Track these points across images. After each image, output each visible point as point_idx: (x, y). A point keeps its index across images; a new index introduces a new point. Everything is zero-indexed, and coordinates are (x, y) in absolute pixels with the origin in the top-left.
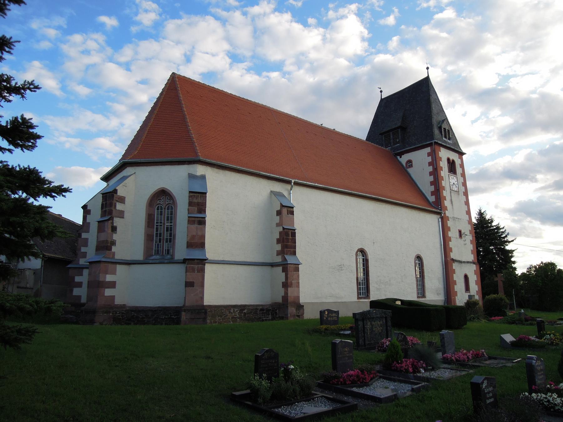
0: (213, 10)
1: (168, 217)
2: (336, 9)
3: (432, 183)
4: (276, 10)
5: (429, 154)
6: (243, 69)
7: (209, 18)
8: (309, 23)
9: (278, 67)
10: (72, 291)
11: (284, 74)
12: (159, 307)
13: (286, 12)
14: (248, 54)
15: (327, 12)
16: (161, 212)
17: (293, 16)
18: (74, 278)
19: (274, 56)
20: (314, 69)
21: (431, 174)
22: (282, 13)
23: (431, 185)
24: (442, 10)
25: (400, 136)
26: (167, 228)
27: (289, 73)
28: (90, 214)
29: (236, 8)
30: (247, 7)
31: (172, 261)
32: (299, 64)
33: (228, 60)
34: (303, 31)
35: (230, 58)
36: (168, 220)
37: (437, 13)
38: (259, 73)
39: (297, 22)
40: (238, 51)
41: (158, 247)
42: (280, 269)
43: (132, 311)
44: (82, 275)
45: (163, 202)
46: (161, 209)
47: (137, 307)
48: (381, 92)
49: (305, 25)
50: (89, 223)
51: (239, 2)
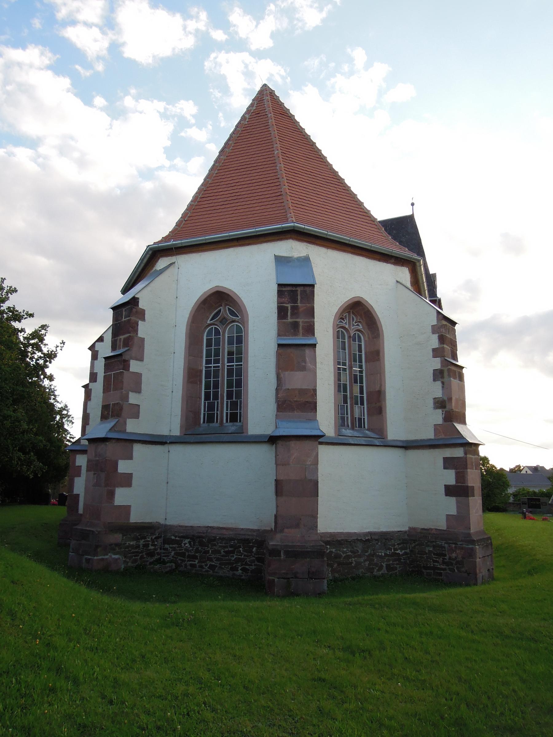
2: (137, 98)
3: (436, 353)
4: (49, 67)
9: (32, 143)
10: (112, 494)
12: (370, 533)
17: (74, 84)
19: (29, 126)
20: (82, 163)
23: (435, 356)
28: (434, 350)
30: (7, 47)
31: (241, 438)
32: (63, 150)
44: (130, 457)
45: (354, 326)
50: (143, 340)
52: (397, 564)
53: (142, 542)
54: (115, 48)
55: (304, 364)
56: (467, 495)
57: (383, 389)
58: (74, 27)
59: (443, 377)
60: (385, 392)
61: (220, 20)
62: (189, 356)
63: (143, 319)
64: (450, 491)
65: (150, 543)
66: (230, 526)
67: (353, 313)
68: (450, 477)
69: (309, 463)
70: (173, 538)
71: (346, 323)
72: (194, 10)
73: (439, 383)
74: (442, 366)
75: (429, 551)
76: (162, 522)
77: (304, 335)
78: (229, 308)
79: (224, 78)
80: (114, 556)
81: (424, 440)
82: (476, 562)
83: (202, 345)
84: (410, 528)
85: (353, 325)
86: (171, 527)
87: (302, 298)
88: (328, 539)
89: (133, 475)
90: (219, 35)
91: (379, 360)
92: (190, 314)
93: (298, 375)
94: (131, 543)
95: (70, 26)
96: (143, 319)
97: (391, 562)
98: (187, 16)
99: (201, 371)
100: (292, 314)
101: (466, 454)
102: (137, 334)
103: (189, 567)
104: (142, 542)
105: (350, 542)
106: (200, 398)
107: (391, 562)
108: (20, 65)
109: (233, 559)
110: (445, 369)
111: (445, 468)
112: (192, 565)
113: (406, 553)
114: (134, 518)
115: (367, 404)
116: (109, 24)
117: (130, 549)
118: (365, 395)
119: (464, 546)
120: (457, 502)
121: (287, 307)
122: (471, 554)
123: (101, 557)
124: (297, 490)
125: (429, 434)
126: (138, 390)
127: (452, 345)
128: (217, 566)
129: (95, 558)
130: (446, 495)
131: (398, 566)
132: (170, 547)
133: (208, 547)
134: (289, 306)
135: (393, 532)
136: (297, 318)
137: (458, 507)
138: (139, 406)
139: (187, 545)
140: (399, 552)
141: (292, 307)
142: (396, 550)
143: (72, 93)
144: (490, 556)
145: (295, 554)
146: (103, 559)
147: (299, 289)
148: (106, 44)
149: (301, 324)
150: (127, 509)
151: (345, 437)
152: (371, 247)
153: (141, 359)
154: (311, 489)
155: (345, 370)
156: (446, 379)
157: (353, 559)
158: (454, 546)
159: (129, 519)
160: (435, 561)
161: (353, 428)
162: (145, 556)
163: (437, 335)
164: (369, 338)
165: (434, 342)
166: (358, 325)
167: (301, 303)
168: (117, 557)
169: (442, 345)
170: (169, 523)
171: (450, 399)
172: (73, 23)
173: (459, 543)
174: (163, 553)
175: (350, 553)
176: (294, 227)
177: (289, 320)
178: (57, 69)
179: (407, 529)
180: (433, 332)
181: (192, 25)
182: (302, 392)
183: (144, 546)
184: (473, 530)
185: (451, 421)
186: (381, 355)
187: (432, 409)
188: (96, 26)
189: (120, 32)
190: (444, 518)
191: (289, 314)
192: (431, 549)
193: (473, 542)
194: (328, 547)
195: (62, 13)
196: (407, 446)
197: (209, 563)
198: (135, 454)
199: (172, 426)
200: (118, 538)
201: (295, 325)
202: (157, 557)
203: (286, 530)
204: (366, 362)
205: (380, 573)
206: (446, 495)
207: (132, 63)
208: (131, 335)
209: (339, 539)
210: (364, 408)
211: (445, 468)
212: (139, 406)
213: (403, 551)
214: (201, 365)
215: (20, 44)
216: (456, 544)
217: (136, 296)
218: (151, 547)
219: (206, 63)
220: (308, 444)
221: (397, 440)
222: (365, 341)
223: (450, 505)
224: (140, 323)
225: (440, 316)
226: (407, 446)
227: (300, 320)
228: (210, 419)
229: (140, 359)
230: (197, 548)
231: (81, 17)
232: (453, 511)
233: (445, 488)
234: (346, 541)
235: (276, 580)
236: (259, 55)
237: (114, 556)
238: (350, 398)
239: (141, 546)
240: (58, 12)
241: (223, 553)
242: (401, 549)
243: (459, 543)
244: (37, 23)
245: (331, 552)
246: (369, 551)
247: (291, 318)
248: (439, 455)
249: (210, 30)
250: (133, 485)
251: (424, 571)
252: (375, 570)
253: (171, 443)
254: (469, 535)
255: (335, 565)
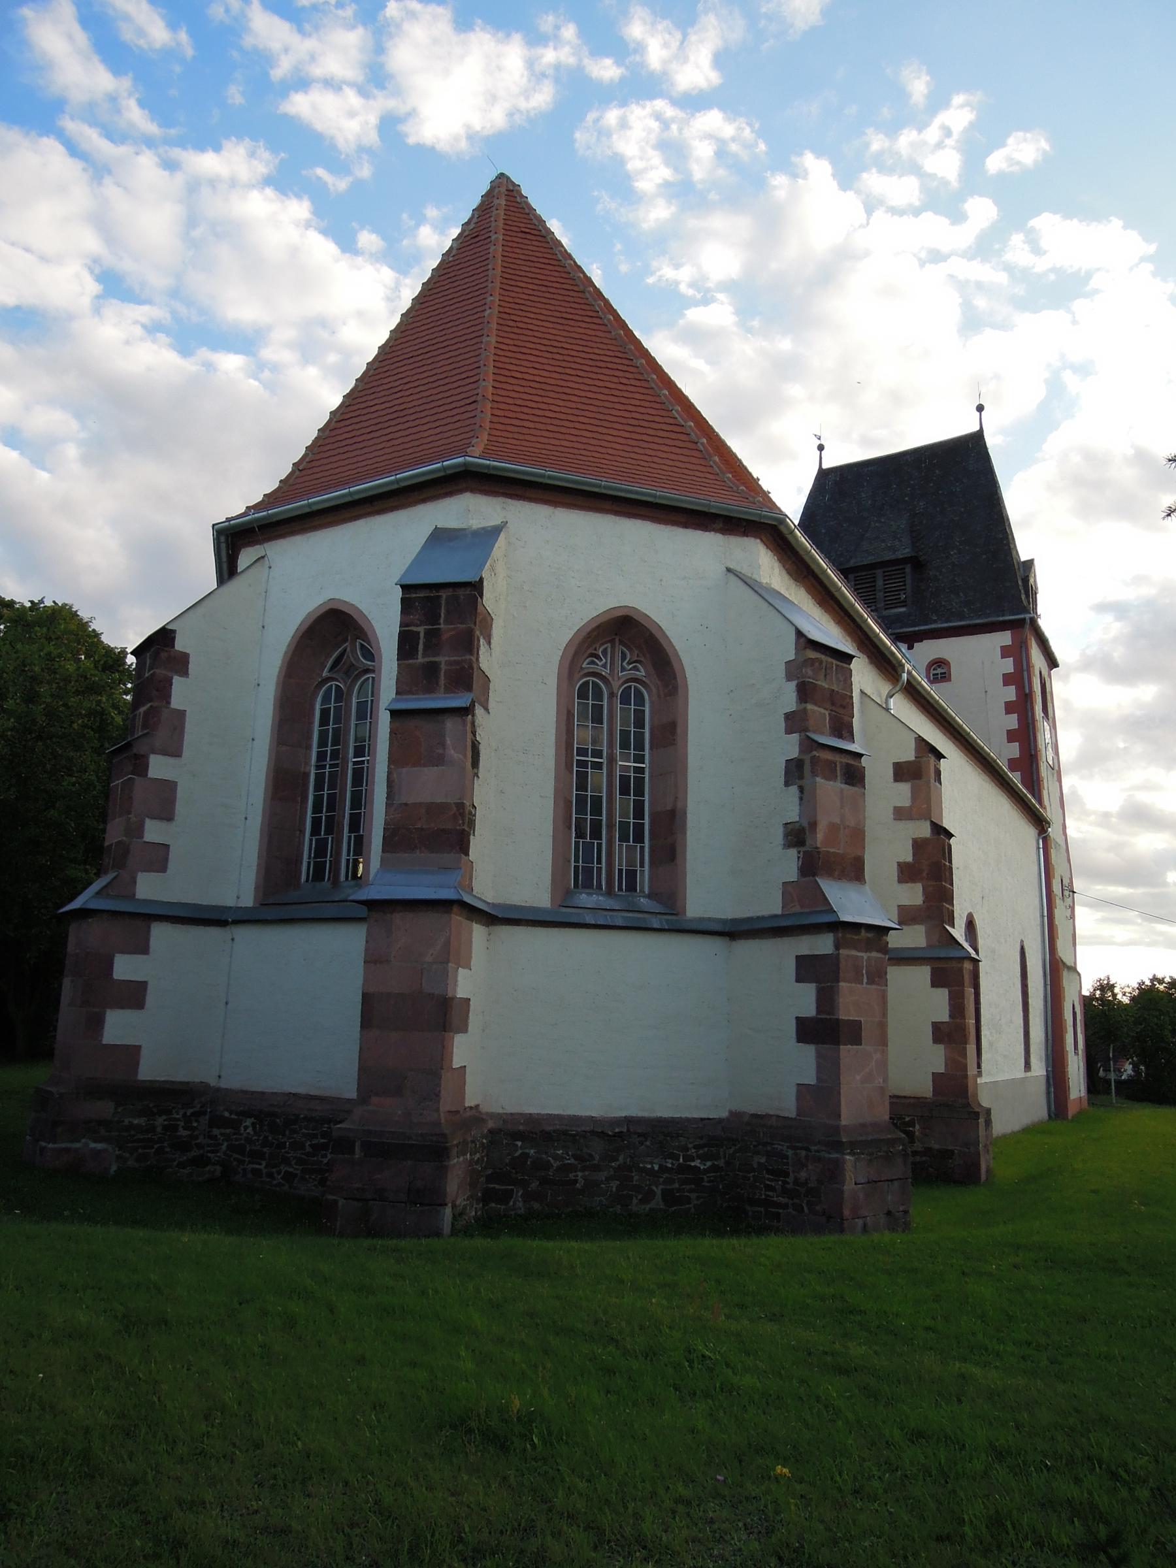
0: (71, 126)
1: (625, 735)
4: (268, 181)
5: (1005, 652)
6: (136, 322)
7: (51, 145)
8: (360, 245)
9: (244, 341)
10: (96, 1023)
11: (258, 368)
12: (629, 1120)
13: (298, 196)
14: (159, 281)
15: (418, 226)
16: (598, 709)
17: (317, 212)
18: (108, 965)
19: (241, 308)
21: (1009, 708)
22: (286, 195)
23: (1009, 741)
24: (706, 300)
25: (908, 587)
26: (624, 780)
27: (275, 368)
28: (788, 717)
29: (149, 142)
30: (185, 148)
33: (93, 287)
34: (337, 260)
35: (99, 279)
36: (625, 745)
37: (696, 303)
38: (185, 351)
39: (325, 232)
40: (126, 265)
41: (588, 859)
42: (923, 973)
43: (516, 1135)
44: (144, 949)
45: (619, 669)
46: (598, 695)
47: (531, 1119)
48: (821, 448)
49: (347, 245)
50: (182, 714)
51: (160, 126)
52: (691, 1191)
53: (160, 1121)
54: (391, 126)
55: (440, 751)
56: (836, 1041)
57: (679, 805)
58: (306, 93)
59: (801, 777)
60: (685, 813)
61: (604, 37)
62: (279, 744)
63: (184, 673)
64: (807, 1031)
65: (182, 1124)
66: (327, 1094)
67: (621, 642)
68: (805, 1000)
69: (429, 959)
70: (227, 1114)
71: (604, 666)
72: (547, 22)
73: (794, 790)
74: (801, 752)
75: (759, 1163)
76: (213, 1082)
77: (448, 690)
78: (362, 646)
79: (619, 161)
80: (93, 1145)
81: (762, 918)
82: (842, 1192)
83: (311, 723)
84: (731, 1113)
85: (623, 669)
86: (228, 1091)
87: (448, 612)
88: (521, 1128)
89: (149, 987)
90: (607, 70)
91: (673, 743)
92: (283, 660)
93: (429, 774)
94: (136, 1122)
95: (297, 92)
96: (184, 673)
97: (677, 1185)
98: (535, 39)
99: (307, 775)
100: (427, 647)
101: (837, 946)
102: (169, 703)
103: (250, 1176)
104: (160, 1121)
105: (574, 1135)
106: (302, 832)
107: (677, 1185)
108: (213, 182)
109: (325, 1161)
110: (807, 758)
111: (798, 981)
112: (254, 1171)
113: (714, 1168)
114: (148, 1071)
115: (651, 839)
116: (376, 77)
117: (133, 1132)
118: (647, 821)
119: (822, 1154)
120: (819, 1056)
121: (418, 633)
122: (834, 1172)
123: (63, 1145)
124: (411, 1017)
125: (771, 905)
126: (167, 815)
127: (833, 704)
128: (296, 1175)
129: (51, 1146)
130: (799, 1041)
131: (693, 1196)
132: (221, 1134)
133: (284, 1135)
134: (421, 630)
135: (688, 1120)
136: (437, 655)
137: (819, 1069)
138: (167, 847)
139: (250, 1130)
140: (697, 1163)
141: (428, 633)
142: (688, 1158)
143: (316, 229)
144: (896, 1184)
145: (383, 1149)
146: (67, 1150)
147: (444, 594)
148: (373, 119)
149: (443, 667)
150: (133, 1052)
151: (573, 910)
152: (655, 496)
153: (176, 752)
154: (445, 1015)
155: (598, 766)
156: (806, 782)
157: (580, 1174)
158: (803, 1153)
159: (136, 1072)
160: (769, 1188)
161: (610, 892)
162: (168, 1149)
163: (794, 683)
164: (659, 696)
165: (789, 699)
166: (635, 669)
167: (446, 622)
168: (99, 1146)
169: (803, 705)
170: (224, 1084)
171: (813, 825)
172: (301, 82)
173: (813, 1148)
174: (209, 1146)
175: (572, 1161)
176: (465, 464)
177: (420, 659)
178: (283, 182)
179: (724, 1114)
180: (789, 677)
181: (549, 56)
182: (434, 809)
183: (165, 1128)
184: (847, 1118)
185: (814, 875)
186: (679, 730)
187: (780, 847)
188: (352, 85)
189: (398, 93)
190: (794, 1090)
191: (421, 647)
192: (763, 1160)
193: (838, 1146)
194: (519, 1144)
195: (282, 69)
196: (734, 931)
197: (284, 1168)
198: (154, 943)
199: (239, 887)
200: (105, 1108)
201: (431, 670)
202: (195, 1153)
203: (374, 1100)
204: (651, 748)
205: (648, 1207)
206: (799, 1041)
207: (426, 153)
208: (155, 704)
209: (548, 1128)
210: (600, 845)
211: (798, 981)
212: (167, 847)
213: (709, 1164)
214: (307, 763)
215: (209, 141)
216: (807, 1149)
217: (169, 627)
218: (183, 1133)
219: (578, 135)
220: (431, 919)
221: (709, 919)
222: (652, 702)
223: (803, 1063)
224: (177, 680)
225: (802, 640)
226: (734, 931)
227: (442, 660)
228: (318, 874)
229: (175, 752)
230: (266, 1137)
231: (317, 71)
232: (810, 1078)
233: (797, 1024)
234: (565, 1133)
235: (341, 1202)
236: (694, 102)
237: (93, 1145)
238: (607, 826)
239: (159, 1129)
240: (272, 68)
241: (308, 1149)
242: (704, 1158)
243: (813, 1148)
244: (235, 95)
245: (525, 1156)
246: (621, 1158)
247: (424, 656)
248: (784, 953)
249: (586, 61)
250: (147, 1006)
251: (748, 1208)
252: (635, 1201)
253: (236, 922)
254: (837, 1129)
255: (534, 1185)
